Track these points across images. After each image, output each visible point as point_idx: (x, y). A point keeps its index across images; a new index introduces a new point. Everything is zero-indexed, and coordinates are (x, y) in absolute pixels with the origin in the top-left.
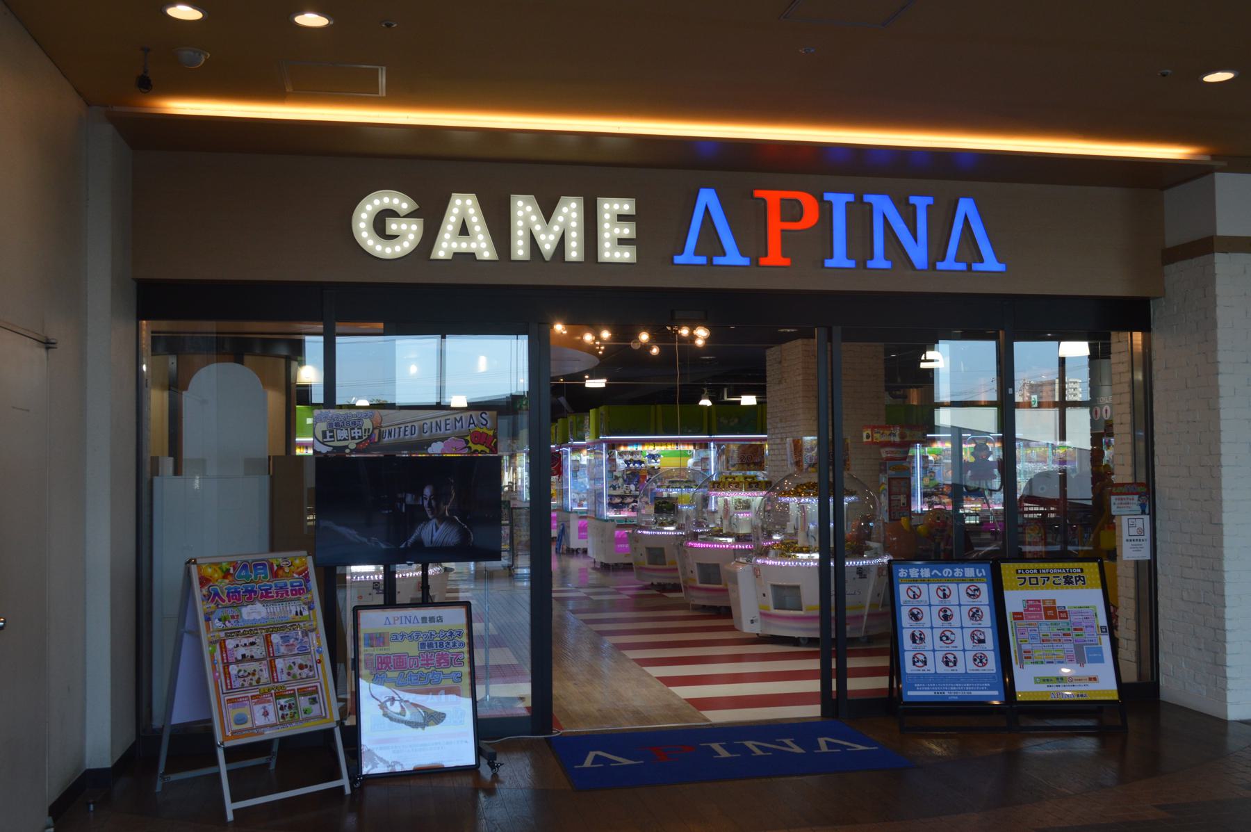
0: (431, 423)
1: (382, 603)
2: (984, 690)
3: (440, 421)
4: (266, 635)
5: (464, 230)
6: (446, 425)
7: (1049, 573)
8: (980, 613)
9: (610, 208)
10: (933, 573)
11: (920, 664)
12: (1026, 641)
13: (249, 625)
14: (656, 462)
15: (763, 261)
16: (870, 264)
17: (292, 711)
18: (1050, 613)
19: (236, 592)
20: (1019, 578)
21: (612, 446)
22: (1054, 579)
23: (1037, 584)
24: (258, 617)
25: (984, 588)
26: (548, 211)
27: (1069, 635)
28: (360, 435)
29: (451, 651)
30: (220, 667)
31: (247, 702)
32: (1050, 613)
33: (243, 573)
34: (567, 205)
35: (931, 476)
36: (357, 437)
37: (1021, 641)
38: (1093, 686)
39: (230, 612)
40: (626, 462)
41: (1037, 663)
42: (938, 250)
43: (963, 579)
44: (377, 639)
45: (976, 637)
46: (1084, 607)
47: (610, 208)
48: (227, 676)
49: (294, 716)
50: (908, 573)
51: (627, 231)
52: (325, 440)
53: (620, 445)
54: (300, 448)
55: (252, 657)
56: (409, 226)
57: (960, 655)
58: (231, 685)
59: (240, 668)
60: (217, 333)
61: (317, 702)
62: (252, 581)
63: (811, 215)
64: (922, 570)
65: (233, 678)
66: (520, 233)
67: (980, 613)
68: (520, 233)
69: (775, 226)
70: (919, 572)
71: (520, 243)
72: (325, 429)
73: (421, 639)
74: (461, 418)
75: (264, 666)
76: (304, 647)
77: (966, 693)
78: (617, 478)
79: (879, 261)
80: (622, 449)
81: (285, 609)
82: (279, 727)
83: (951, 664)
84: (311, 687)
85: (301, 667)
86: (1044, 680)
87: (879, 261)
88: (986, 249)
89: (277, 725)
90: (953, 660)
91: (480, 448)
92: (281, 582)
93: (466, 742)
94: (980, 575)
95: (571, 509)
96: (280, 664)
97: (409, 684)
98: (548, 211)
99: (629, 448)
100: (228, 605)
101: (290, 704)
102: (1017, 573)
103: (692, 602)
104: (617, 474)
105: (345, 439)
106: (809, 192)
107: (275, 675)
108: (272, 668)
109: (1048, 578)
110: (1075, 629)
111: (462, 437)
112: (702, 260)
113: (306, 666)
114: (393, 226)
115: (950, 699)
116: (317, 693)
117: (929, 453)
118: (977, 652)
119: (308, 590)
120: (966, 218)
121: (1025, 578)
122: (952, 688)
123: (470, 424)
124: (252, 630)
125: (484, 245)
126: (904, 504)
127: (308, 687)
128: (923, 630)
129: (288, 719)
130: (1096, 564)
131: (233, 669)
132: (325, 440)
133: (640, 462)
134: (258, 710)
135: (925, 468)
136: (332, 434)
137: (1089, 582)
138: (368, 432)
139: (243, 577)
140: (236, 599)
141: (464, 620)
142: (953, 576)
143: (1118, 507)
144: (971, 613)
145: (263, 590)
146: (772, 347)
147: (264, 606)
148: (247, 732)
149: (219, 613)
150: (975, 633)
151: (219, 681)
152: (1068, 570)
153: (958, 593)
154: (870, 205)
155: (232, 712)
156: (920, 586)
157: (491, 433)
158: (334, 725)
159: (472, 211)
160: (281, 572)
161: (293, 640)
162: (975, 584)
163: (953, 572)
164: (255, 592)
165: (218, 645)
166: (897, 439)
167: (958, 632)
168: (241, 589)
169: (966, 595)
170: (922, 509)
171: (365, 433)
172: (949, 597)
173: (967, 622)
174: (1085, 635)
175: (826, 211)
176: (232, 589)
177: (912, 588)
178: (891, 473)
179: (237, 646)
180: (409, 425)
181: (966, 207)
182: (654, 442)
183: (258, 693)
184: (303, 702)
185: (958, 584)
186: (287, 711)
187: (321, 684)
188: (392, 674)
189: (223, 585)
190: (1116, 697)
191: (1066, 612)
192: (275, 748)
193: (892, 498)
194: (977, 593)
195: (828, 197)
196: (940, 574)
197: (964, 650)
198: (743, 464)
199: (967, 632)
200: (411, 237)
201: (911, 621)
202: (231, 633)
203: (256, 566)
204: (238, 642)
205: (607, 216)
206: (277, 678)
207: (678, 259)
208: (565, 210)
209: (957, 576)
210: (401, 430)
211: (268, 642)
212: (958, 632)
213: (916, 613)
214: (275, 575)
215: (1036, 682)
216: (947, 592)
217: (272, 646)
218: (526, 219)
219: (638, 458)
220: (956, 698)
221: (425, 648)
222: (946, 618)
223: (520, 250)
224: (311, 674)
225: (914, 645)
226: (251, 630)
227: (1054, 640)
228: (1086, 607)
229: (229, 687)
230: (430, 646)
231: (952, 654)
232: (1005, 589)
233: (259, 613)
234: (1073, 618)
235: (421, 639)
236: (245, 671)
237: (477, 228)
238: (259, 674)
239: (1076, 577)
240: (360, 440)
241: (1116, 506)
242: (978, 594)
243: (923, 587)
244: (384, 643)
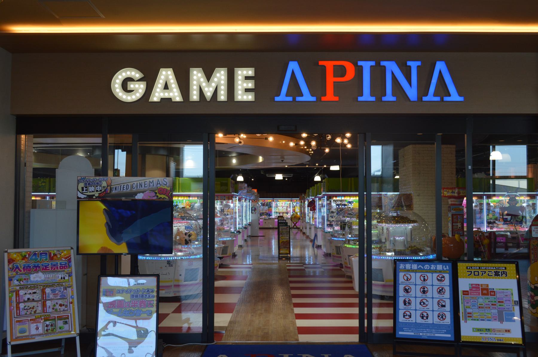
0: (137, 183)
1: (129, 274)
2: (443, 334)
3: (142, 183)
4: (43, 289)
5: (166, 87)
6: (145, 184)
7: (486, 269)
8: (444, 290)
9: (241, 73)
10: (419, 267)
11: (407, 317)
12: (469, 307)
13: (34, 283)
14: (351, 205)
15: (324, 99)
16: (384, 99)
17: (53, 327)
18: (485, 292)
19: (28, 266)
20: (467, 271)
21: (329, 197)
22: (488, 273)
23: (478, 275)
24: (39, 280)
25: (447, 276)
26: (209, 76)
27: (495, 305)
28: (101, 189)
29: (147, 299)
30: (14, 304)
31: (28, 322)
32: (485, 292)
33: (34, 257)
34: (219, 72)
35: (493, 214)
36: (99, 191)
37: (466, 307)
38: (507, 335)
39: (24, 277)
40: (337, 205)
41: (475, 320)
42: (423, 89)
43: (435, 271)
44: (111, 292)
45: (440, 304)
46: (505, 289)
47: (241, 73)
48: (18, 309)
49: (53, 330)
50: (405, 267)
51: (250, 85)
52: (83, 192)
53: (333, 197)
54: (186, 197)
55: (33, 299)
56: (139, 86)
57: (430, 313)
58: (19, 313)
59: (25, 305)
60: (114, 144)
61: (67, 324)
62: (38, 262)
63: (351, 73)
64: (413, 265)
65: (21, 310)
66: (195, 87)
67: (444, 290)
68: (195, 87)
69: (331, 80)
70: (411, 266)
71: (195, 92)
72: (83, 186)
73: (132, 293)
74: (153, 181)
75: (40, 304)
76: (64, 295)
77: (432, 335)
78: (333, 212)
79: (389, 97)
80: (334, 198)
81: (55, 276)
82: (44, 335)
83: (425, 318)
84: (65, 316)
85: (61, 305)
86: (478, 330)
87: (389, 97)
88: (452, 89)
89: (43, 335)
90: (426, 315)
91: (163, 196)
92: (54, 263)
93: (151, 347)
94: (445, 269)
95: (318, 227)
96: (48, 303)
97: (124, 316)
98: (209, 76)
99: (338, 198)
100: (23, 273)
101: (52, 324)
102: (467, 268)
103: (346, 274)
104: (333, 210)
105: (93, 192)
106: (350, 62)
107: (45, 309)
108: (44, 305)
109: (485, 272)
110: (499, 302)
111: (153, 191)
112: (290, 99)
113: (64, 305)
114: (131, 86)
115: (423, 337)
116: (68, 318)
117: (492, 202)
118: (440, 312)
119: (70, 267)
120: (440, 72)
121: (471, 272)
122: (424, 332)
123: (157, 184)
124: (35, 286)
125: (176, 94)
126: (460, 228)
127: (63, 316)
128: (411, 298)
129: (50, 331)
130: (514, 265)
131: (22, 306)
132: (83, 192)
133: (345, 205)
134: (33, 326)
135: (488, 210)
136: (86, 189)
137: (509, 275)
138: (105, 188)
139: (34, 259)
140: (28, 270)
141: (155, 284)
142: (430, 269)
143: (536, 233)
144: (439, 290)
145: (44, 266)
146: (401, 149)
147: (43, 274)
148: (25, 337)
149: (18, 277)
150: (440, 301)
151: (13, 311)
152: (497, 268)
153: (432, 278)
154: (385, 67)
155: (19, 327)
156: (428, 274)
157: (169, 189)
158: (75, 335)
159: (171, 77)
160: (55, 257)
161: (58, 291)
162: (442, 274)
163: (430, 267)
164: (39, 267)
165: (14, 294)
166: (456, 195)
167: (430, 300)
168: (32, 265)
169: (436, 280)
170: (486, 230)
171: (103, 188)
172: (427, 280)
173: (436, 295)
174: (505, 305)
175: (359, 71)
176: (27, 265)
177: (406, 275)
178: (453, 212)
179: (26, 294)
180: (126, 184)
181: (440, 66)
182: (350, 196)
183: (34, 318)
184: (60, 323)
185: (432, 273)
186: (50, 328)
187: (71, 314)
188: (115, 310)
189: (21, 263)
190: (521, 342)
191: (494, 292)
192: (63, 344)
193: (454, 224)
194: (443, 279)
195: (360, 63)
196: (423, 268)
197: (433, 311)
198: (398, 206)
199: (436, 301)
200: (140, 91)
201: (404, 293)
202: (23, 287)
203: (41, 254)
204: (26, 292)
205: (240, 77)
206: (46, 311)
207: (277, 99)
208: (218, 75)
209: (432, 269)
210: (122, 187)
211: (43, 292)
212: (430, 300)
213: (408, 289)
214: (51, 258)
215: (473, 331)
216: (426, 278)
217: (45, 294)
218: (198, 80)
219: (344, 203)
220: (426, 337)
221: (134, 297)
222: (424, 292)
223: (195, 96)
224: (66, 309)
225: (405, 306)
226: (34, 286)
227: (486, 307)
228: (507, 290)
229: (18, 314)
230: (137, 296)
231: (410, 312)
232: (459, 277)
233: (40, 277)
234: (498, 295)
235: (132, 293)
236: (28, 307)
237: (173, 86)
238: (36, 308)
239: (501, 272)
240: (101, 192)
241: (535, 232)
242: (443, 279)
243: (413, 274)
244: (113, 294)
